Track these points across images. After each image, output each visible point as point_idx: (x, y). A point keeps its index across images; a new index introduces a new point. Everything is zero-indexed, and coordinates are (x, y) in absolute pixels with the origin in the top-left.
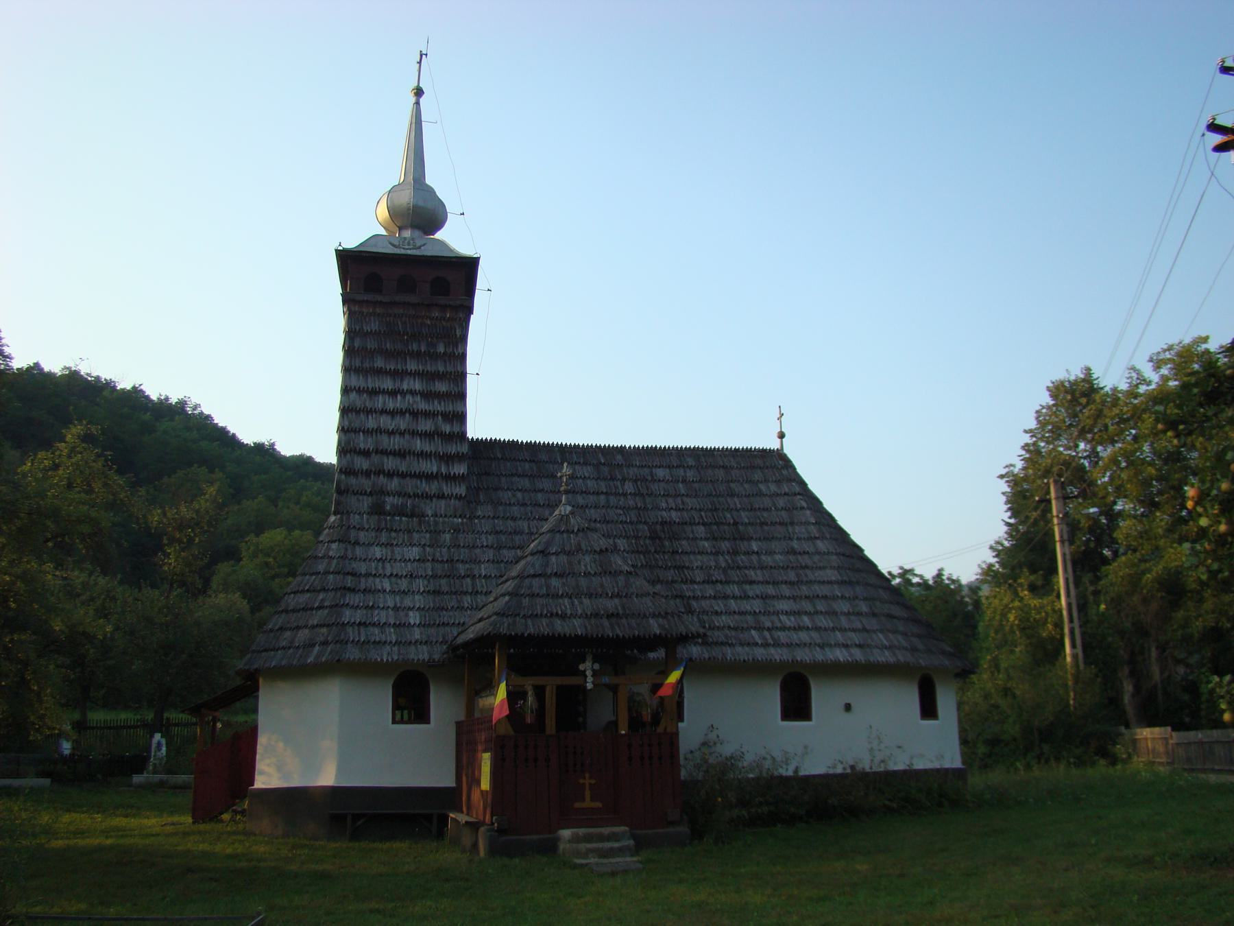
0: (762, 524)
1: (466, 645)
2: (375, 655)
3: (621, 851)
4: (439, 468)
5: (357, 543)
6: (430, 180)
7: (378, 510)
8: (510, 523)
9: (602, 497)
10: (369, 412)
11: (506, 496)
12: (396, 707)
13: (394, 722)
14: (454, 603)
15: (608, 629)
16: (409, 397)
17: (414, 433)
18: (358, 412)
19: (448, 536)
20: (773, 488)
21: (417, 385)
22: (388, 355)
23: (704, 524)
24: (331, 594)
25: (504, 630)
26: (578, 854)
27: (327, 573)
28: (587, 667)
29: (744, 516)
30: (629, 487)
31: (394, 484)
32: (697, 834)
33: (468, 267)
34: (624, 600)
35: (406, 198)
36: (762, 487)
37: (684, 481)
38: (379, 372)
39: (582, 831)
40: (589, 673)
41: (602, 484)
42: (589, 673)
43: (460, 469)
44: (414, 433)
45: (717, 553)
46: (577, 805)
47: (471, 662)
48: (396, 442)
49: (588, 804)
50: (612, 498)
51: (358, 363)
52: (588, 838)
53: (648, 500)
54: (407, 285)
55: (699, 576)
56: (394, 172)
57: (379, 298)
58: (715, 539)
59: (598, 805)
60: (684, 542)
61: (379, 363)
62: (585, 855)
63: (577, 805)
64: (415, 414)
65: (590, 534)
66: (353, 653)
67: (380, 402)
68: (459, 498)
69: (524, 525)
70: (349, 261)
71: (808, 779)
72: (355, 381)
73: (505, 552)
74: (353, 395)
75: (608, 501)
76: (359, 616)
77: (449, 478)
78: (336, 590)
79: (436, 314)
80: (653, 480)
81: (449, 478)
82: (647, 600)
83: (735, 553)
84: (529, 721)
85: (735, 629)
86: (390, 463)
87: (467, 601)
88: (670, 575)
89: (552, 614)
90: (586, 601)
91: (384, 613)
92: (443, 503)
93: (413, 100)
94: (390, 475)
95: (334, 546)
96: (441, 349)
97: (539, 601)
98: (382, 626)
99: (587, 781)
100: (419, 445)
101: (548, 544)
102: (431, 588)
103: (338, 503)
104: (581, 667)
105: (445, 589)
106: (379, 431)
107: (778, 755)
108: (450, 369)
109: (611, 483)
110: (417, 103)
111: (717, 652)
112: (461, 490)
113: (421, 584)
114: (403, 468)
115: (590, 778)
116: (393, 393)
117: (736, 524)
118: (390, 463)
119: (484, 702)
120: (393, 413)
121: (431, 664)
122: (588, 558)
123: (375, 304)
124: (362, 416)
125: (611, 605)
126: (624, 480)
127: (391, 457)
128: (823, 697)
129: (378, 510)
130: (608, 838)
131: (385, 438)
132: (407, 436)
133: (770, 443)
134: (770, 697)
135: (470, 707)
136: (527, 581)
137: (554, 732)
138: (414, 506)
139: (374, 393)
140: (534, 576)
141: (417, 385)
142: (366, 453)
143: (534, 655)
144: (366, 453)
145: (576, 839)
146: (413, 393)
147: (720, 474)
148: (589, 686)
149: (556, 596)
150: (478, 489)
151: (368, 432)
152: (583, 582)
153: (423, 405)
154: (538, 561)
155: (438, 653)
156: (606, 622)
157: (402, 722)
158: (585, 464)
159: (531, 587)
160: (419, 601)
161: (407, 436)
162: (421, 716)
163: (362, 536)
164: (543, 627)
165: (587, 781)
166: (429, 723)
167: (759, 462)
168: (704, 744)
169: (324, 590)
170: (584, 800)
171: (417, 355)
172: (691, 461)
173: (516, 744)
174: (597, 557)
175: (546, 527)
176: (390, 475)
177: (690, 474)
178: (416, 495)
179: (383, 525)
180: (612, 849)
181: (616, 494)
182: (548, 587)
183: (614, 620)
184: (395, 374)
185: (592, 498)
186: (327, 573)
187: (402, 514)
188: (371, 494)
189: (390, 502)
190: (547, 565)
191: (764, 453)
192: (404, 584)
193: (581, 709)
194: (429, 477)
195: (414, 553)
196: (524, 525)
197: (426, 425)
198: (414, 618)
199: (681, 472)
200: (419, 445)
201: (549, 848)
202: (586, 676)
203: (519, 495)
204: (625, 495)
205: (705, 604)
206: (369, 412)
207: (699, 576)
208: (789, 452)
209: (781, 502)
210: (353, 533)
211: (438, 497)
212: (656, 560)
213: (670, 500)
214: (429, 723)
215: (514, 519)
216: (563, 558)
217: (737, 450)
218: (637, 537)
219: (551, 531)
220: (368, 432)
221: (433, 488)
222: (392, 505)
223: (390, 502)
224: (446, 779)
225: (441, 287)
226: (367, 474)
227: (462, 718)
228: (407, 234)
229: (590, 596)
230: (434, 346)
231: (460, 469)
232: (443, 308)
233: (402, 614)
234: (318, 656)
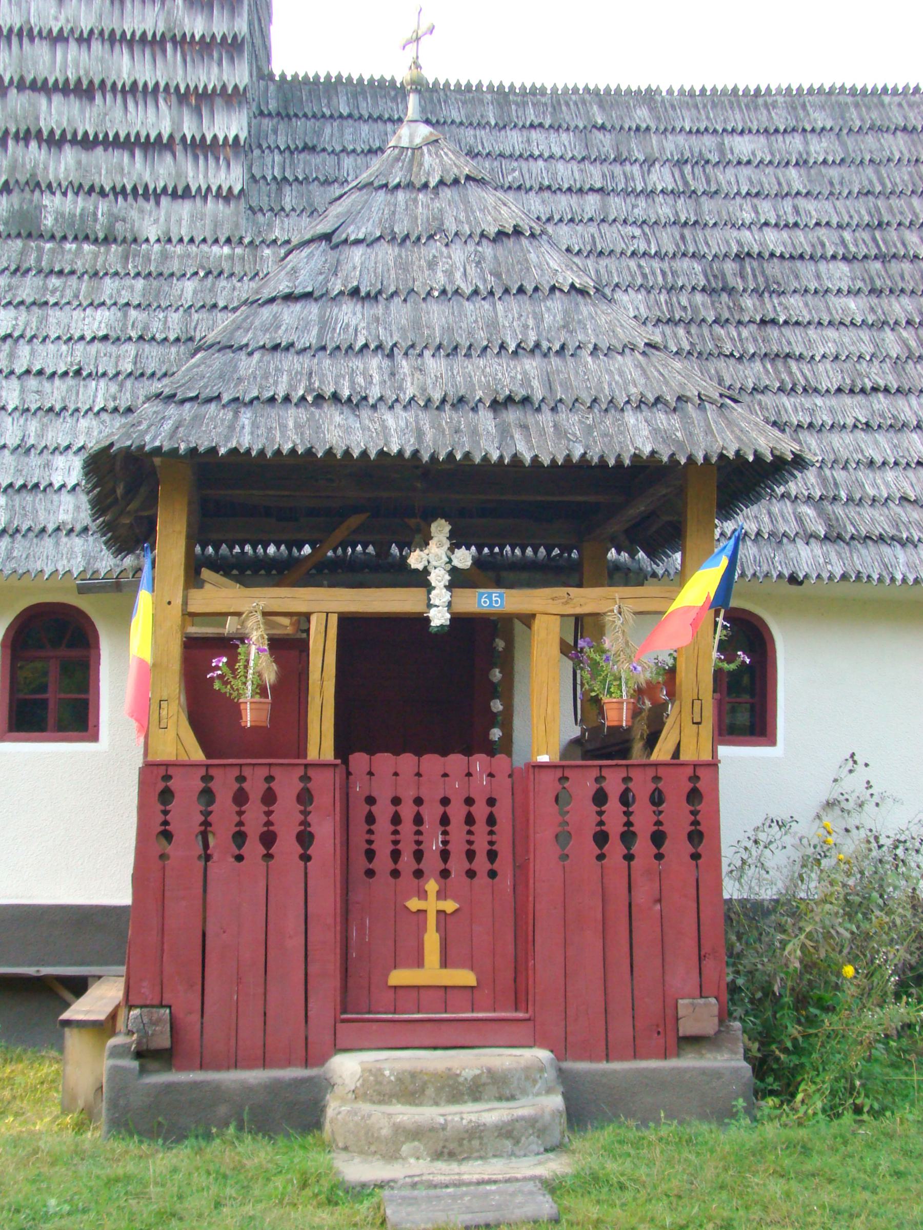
4: (177, 124)
15: (486, 439)
17: (113, 39)
30: (662, 177)
31: (65, 164)
32: (774, 1076)
34: (555, 361)
40: (439, 578)
42: (439, 578)
43: (230, 125)
44: (113, 39)
46: (400, 977)
49: (431, 972)
52: (410, 1089)
53: (707, 204)
55: (829, 376)
58: (875, 291)
59: (466, 977)
63: (400, 977)
65: (473, 191)
68: (227, 197)
75: (604, 207)
77: (202, 148)
81: (202, 148)
82: (627, 363)
84: (248, 719)
86: (55, 114)
89: (319, 398)
92: (185, 208)
94: (55, 141)
97: (290, 362)
99: (431, 902)
100: (126, 67)
104: (416, 560)
109: (617, 169)
111: (866, 560)
112: (233, 177)
113: (99, 393)
115: (441, 895)
118: (55, 114)
126: (649, 162)
127: (57, 99)
130: (475, 1090)
131: (42, 50)
132: (96, 45)
136: (266, 313)
137: (328, 754)
138: (114, 219)
140: (289, 298)
145: (378, 1090)
148: (439, 618)
156: (486, 420)
158: (556, 128)
161: (96, 45)
165: (431, 902)
166: (95, 738)
168: (830, 805)
170: (419, 962)
174: (487, 249)
176: (55, 141)
178: (120, 192)
179: (31, 261)
180: (475, 1133)
181: (627, 193)
183: (512, 415)
189: (54, 208)
192: (56, 393)
193: (497, 706)
199: (796, 142)
200: (126, 67)
201: (298, 1114)
202: (429, 587)
204: (650, 194)
207: (829, 376)
211: (174, 195)
212: (716, 339)
214: (95, 738)
221: (161, 171)
222: (59, 216)
223: (54, 208)
231: (230, 125)
233: (34, 460)
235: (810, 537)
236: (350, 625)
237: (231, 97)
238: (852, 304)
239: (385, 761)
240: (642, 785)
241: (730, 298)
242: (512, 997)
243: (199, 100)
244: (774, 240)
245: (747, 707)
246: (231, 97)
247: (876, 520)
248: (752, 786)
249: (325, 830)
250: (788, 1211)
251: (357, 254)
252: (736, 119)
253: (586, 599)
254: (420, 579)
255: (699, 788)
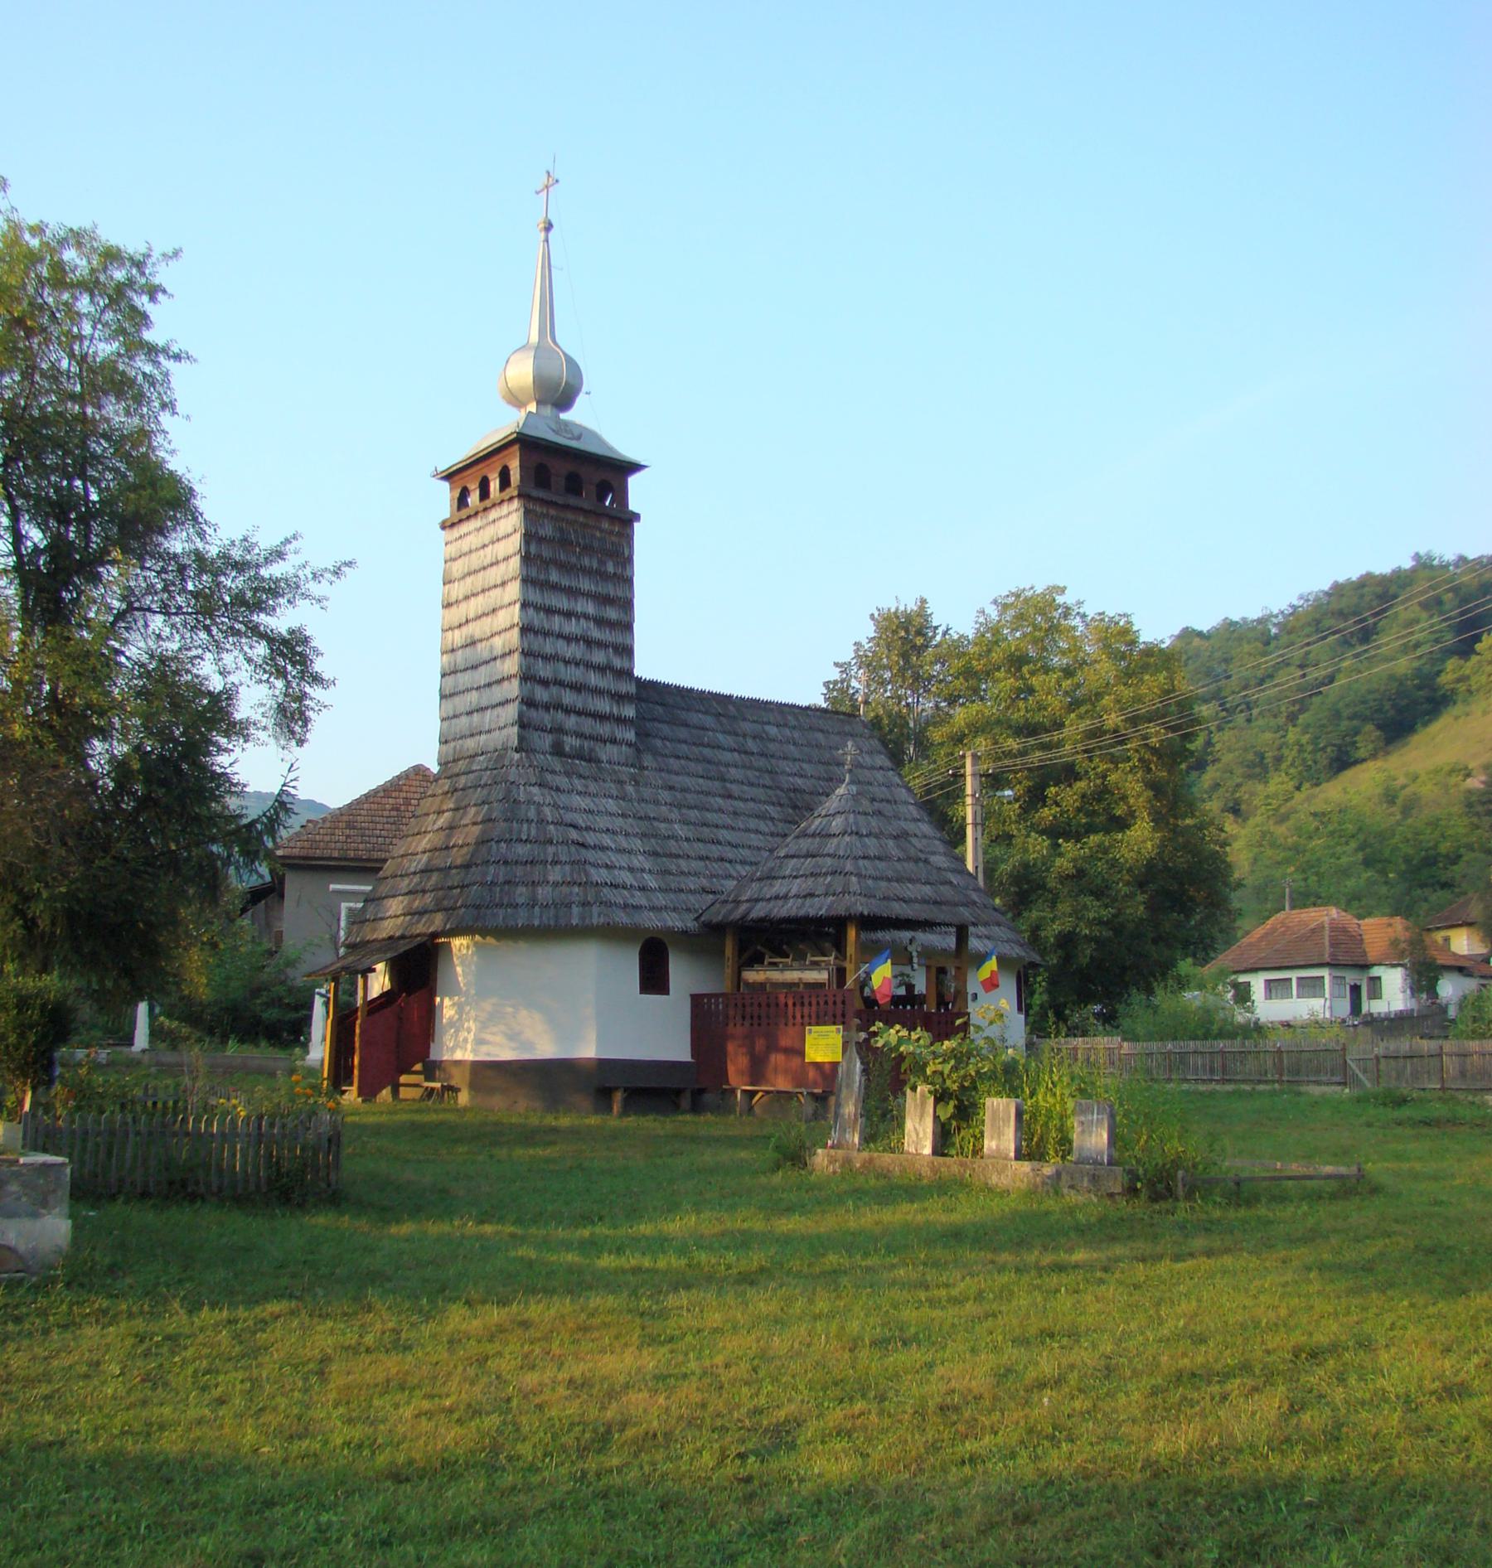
21: (590, 608)
31: (571, 722)
64: (589, 643)
68: (629, 744)
72: (535, 596)
74: (531, 611)
86: (568, 697)
94: (568, 711)
100: (594, 679)
118: (568, 697)
141: (590, 608)
142: (545, 683)
144: (545, 683)
146: (586, 616)
153: (596, 633)
176: (568, 711)
178: (591, 737)
188: (551, 732)
189: (570, 742)
200: (594, 679)
223: (570, 742)
236: (1299, 979)
250: (596, 1309)
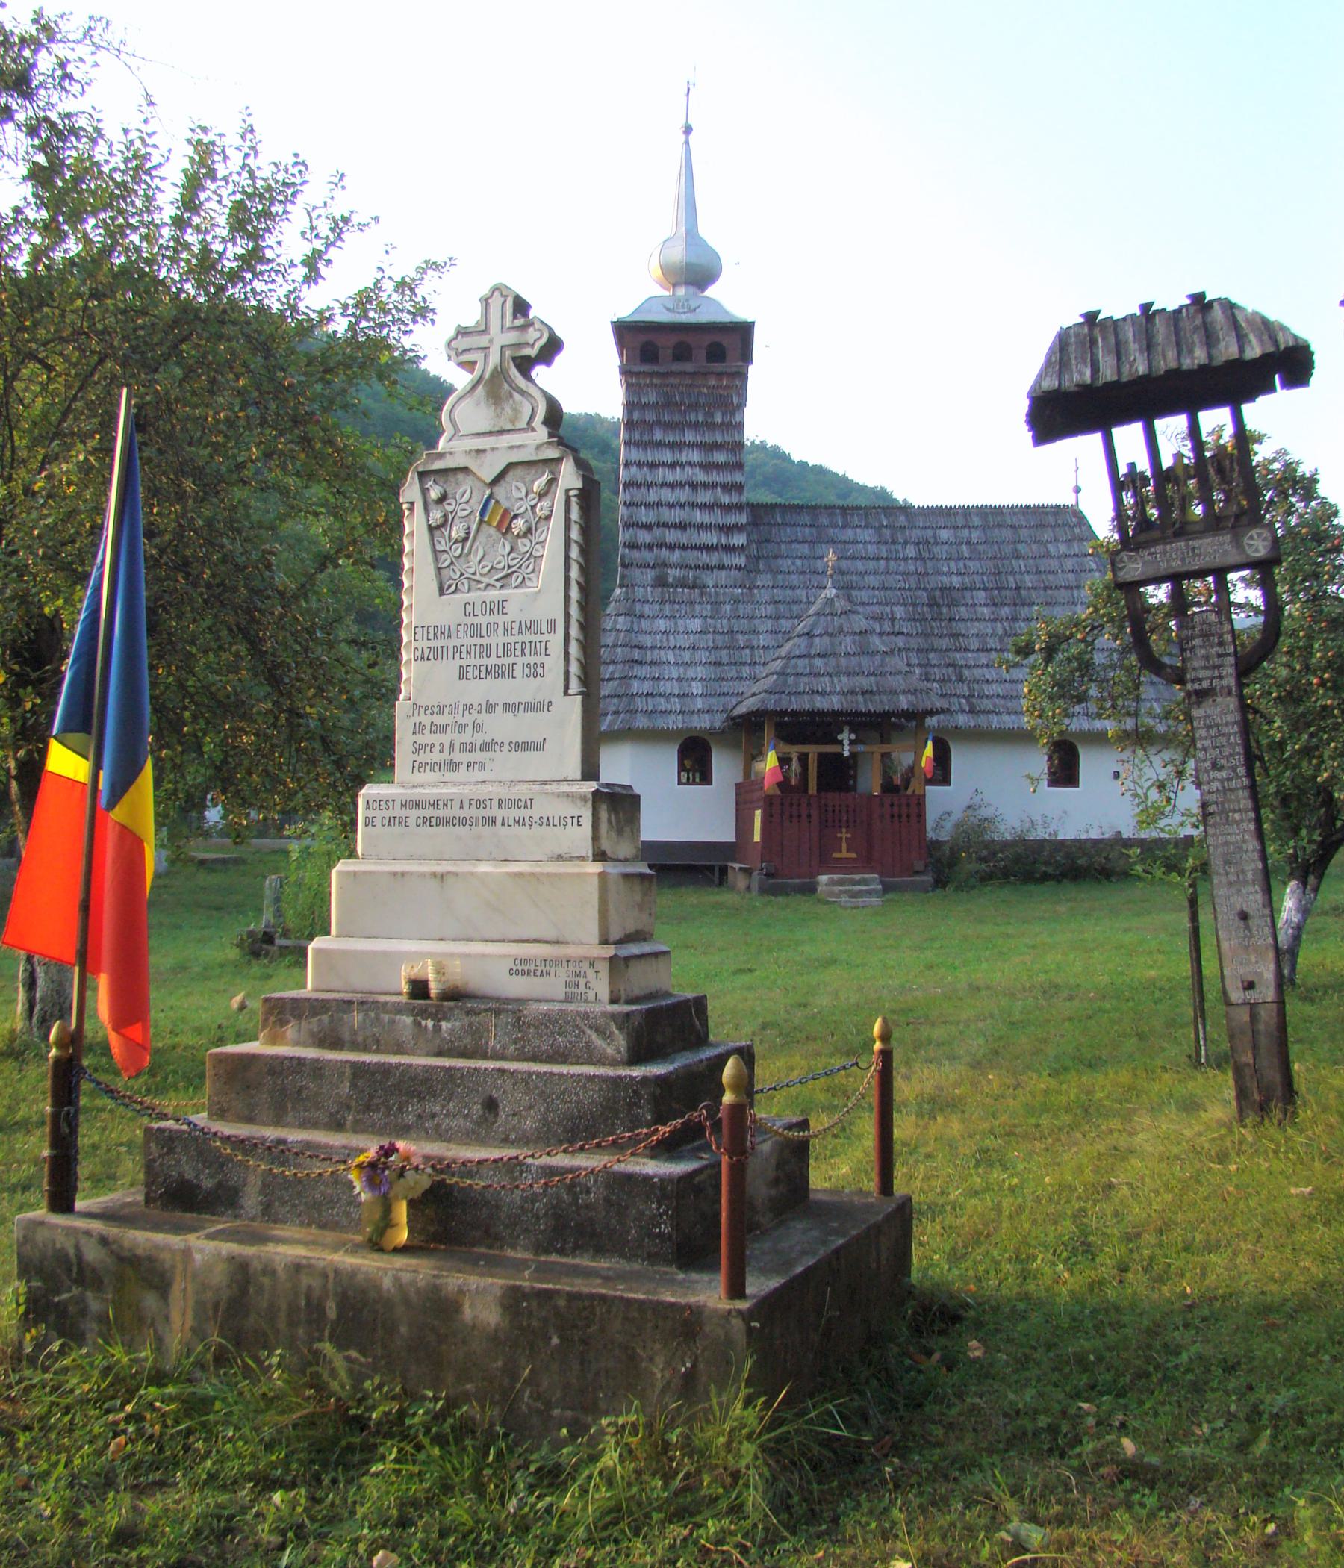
0: (1046, 588)
1: (740, 716)
2: (661, 723)
3: (869, 893)
5: (642, 616)
6: (704, 231)
7: (661, 582)
8: (789, 592)
9: (882, 562)
10: (650, 485)
11: (785, 564)
12: (682, 768)
13: (680, 783)
14: (734, 674)
15: (862, 705)
16: (687, 468)
17: (694, 505)
18: (639, 485)
19: (728, 607)
20: (1063, 548)
21: (696, 456)
22: (667, 426)
23: (985, 589)
24: (620, 667)
25: (771, 707)
26: (832, 894)
27: (615, 645)
28: (845, 737)
29: (1029, 580)
30: (911, 551)
31: (676, 556)
32: (940, 883)
33: (743, 332)
35: (678, 254)
36: (1051, 547)
37: (968, 543)
38: (659, 444)
39: (836, 877)
40: (846, 742)
41: (883, 548)
42: (846, 742)
43: (739, 539)
44: (694, 505)
45: (995, 620)
46: (836, 855)
47: (748, 730)
48: (677, 515)
49: (844, 854)
50: (892, 563)
51: (637, 436)
52: (841, 883)
53: (929, 564)
54: (682, 353)
56: (665, 222)
57: (656, 369)
58: (995, 605)
60: (962, 609)
61: (658, 435)
62: (838, 895)
63: (836, 855)
64: (694, 486)
65: (852, 616)
66: (642, 722)
67: (660, 475)
68: (739, 568)
69: (802, 594)
70: (626, 332)
71: (1063, 842)
73: (783, 622)
76: (646, 687)
77: (729, 549)
78: (625, 662)
79: (712, 382)
80: (936, 543)
81: (729, 549)
83: (1015, 619)
85: (1004, 697)
86: (671, 536)
87: (746, 671)
88: (944, 643)
90: (845, 679)
91: (668, 684)
92: (723, 573)
93: (683, 138)
94: (672, 547)
95: (621, 619)
96: (718, 418)
98: (668, 696)
99: (844, 835)
100: (699, 516)
101: (814, 626)
102: (712, 659)
103: (623, 577)
105: (725, 660)
106: (659, 504)
107: (1037, 818)
108: (728, 438)
110: (687, 142)
111: (982, 721)
112: (741, 560)
113: (702, 656)
114: (684, 541)
116: (673, 466)
117: (1018, 588)
118: (671, 536)
119: (758, 766)
120: (672, 486)
121: (712, 732)
122: (849, 639)
123: (652, 374)
124: (644, 490)
125: (865, 682)
126: (906, 543)
128: (1092, 764)
129: (661, 582)
130: (859, 882)
131: (665, 511)
133: (1066, 499)
134: (1038, 762)
135: (747, 771)
138: (695, 578)
139: (653, 466)
142: (648, 527)
143: (799, 727)
144: (648, 527)
145: (833, 883)
146: (690, 464)
147: (1007, 534)
148: (846, 754)
149: (817, 675)
150: (758, 558)
151: (650, 506)
152: (843, 661)
153: (702, 477)
154: (803, 642)
155: (719, 720)
156: (860, 698)
157: (688, 783)
158: (867, 527)
159: (796, 666)
160: (701, 671)
162: (706, 779)
163: (646, 609)
164: (805, 704)
165: (844, 835)
167: (1051, 520)
169: (613, 662)
171: (695, 426)
172: (977, 521)
173: (783, 804)
175: (813, 610)
176: (672, 547)
177: (975, 535)
178: (697, 567)
182: (811, 666)
184: (674, 446)
185: (871, 564)
186: (615, 645)
187: (684, 586)
189: (673, 574)
190: (811, 645)
191: (1058, 510)
192: (687, 656)
194: (709, 548)
195: (696, 624)
196: (802, 594)
197: (705, 497)
198: (697, 688)
199: (966, 532)
200: (699, 516)
201: (810, 889)
203: (799, 562)
204: (906, 559)
205: (977, 672)
206: (650, 485)
207: (975, 644)
208: (1085, 508)
209: (1069, 564)
210: (638, 606)
213: (952, 564)
215: (793, 588)
216: (826, 639)
217: (1028, 507)
218: (914, 605)
219: (817, 614)
220: (650, 506)
221: (713, 559)
223: (673, 574)
224: (728, 836)
225: (716, 353)
226: (650, 547)
227: (740, 780)
228: (681, 291)
229: (849, 674)
230: (712, 416)
231: (739, 539)
232: (720, 375)
234: (611, 724)
235: (963, 711)
236: (821, 757)
237: (738, 528)
238: (985, 610)
239: (830, 795)
240: (902, 800)
241: (939, 605)
242: (867, 861)
243: (727, 529)
244: (956, 581)
245: (942, 773)
246: (738, 528)
247: (987, 704)
248: (936, 799)
249: (815, 813)
251: (817, 640)
252: (941, 521)
253: (886, 748)
254: (841, 742)
255: (920, 801)
